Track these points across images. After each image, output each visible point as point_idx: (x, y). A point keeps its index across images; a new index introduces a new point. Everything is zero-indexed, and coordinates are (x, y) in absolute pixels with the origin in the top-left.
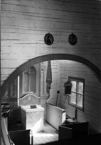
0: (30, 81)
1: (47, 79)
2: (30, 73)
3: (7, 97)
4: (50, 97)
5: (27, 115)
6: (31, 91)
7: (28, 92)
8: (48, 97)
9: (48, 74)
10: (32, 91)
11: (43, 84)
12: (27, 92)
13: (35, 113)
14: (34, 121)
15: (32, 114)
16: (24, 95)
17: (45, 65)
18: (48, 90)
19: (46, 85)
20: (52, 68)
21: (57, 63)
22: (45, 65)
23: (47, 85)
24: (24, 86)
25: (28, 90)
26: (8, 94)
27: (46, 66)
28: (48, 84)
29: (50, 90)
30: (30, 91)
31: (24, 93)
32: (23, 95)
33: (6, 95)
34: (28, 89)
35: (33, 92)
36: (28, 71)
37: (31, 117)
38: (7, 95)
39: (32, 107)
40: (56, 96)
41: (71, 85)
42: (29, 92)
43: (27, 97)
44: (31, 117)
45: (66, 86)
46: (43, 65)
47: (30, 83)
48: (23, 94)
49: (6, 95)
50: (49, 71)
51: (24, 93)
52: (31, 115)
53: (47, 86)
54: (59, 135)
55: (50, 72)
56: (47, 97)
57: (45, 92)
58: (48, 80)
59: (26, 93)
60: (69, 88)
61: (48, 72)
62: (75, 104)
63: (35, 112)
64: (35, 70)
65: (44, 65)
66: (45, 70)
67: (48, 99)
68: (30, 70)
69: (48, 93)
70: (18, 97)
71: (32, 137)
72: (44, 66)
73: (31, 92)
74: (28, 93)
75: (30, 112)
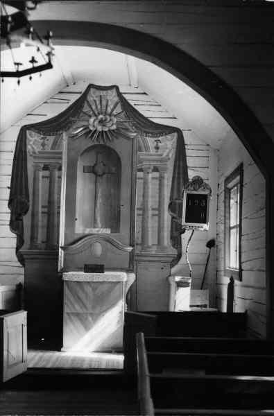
0: (99, 195)
1: (171, 198)
2: (99, 169)
4: (182, 261)
5: (66, 291)
7: (94, 227)
11: (160, 216)
12: (91, 227)
14: (91, 314)
16: (81, 236)
17: (168, 155)
18: (176, 234)
19: (170, 217)
20: (188, 165)
21: (208, 148)
22: (165, 155)
23: (173, 218)
24: (83, 205)
27: (170, 155)
29: (182, 235)
30: (100, 225)
36: (96, 165)
37: (79, 299)
38: (43, 242)
40: (203, 258)
41: (206, 192)
42: (97, 229)
44: (79, 299)
45: (188, 195)
49: (39, 242)
52: (81, 295)
55: (181, 176)
56: (171, 259)
57: (167, 241)
59: (87, 231)
60: (199, 204)
64: (119, 159)
65: (161, 155)
66: (165, 169)
68: (100, 160)
69: (174, 246)
71: (8, 334)
73: (105, 229)
75: (78, 282)
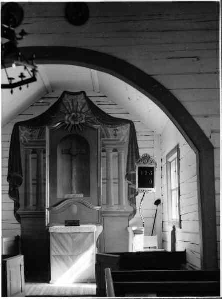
1: (127, 170)
3: (34, 208)
6: (77, 193)
7: (71, 193)
8: (131, 215)
9: (130, 160)
10: (80, 193)
13: (72, 238)
15: (64, 238)
17: (123, 140)
19: (127, 184)
22: (121, 139)
23: (129, 185)
24: (62, 179)
25: (70, 190)
26: (35, 204)
27: (125, 140)
28: (130, 183)
29: (137, 197)
30: (75, 192)
31: (60, 195)
32: (58, 201)
33: (31, 205)
34: (72, 188)
35: (82, 196)
37: (62, 245)
39: (69, 223)
42: (74, 195)
43: (69, 206)
44: (62, 245)
46: (117, 138)
47: (74, 174)
48: (60, 199)
49: (31, 205)
50: (132, 148)
51: (60, 195)
52: (63, 242)
53: (128, 188)
54: (97, 284)
56: (129, 214)
58: (130, 175)
59: (66, 197)
61: (130, 154)
62: (172, 189)
63: (73, 233)
65: (118, 140)
67: (130, 219)
70: (48, 205)
72: (119, 142)
74: (72, 196)
